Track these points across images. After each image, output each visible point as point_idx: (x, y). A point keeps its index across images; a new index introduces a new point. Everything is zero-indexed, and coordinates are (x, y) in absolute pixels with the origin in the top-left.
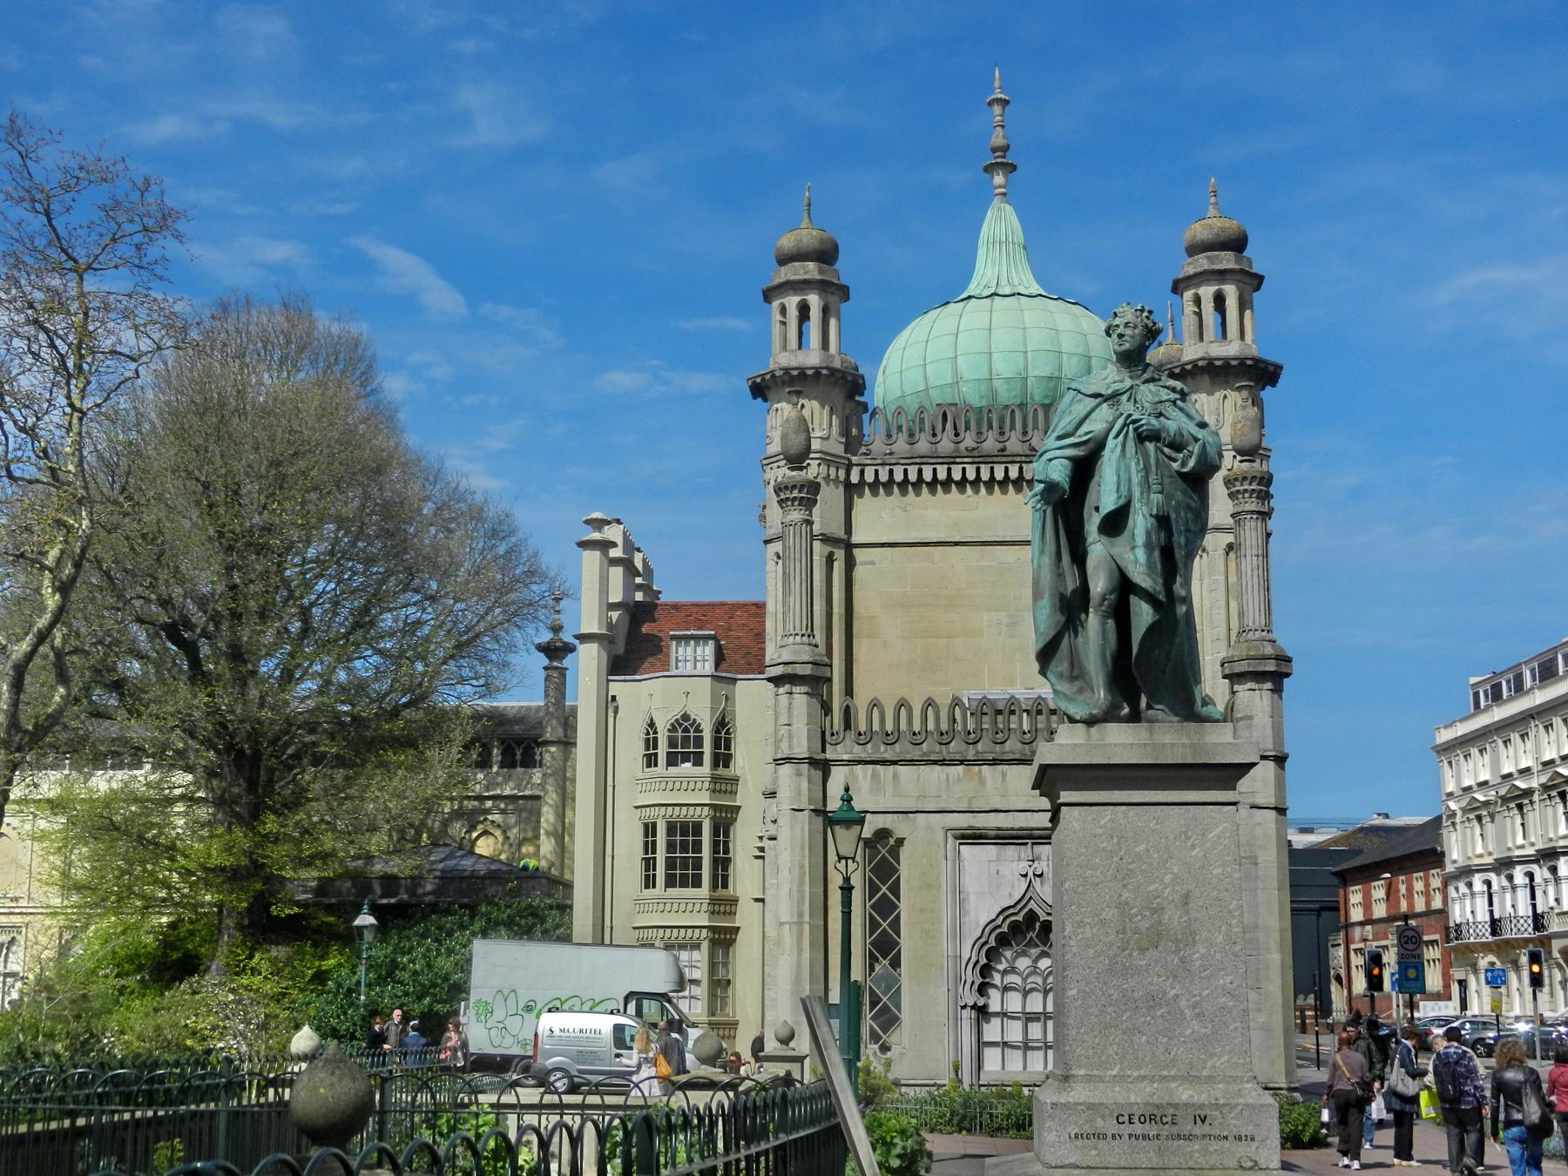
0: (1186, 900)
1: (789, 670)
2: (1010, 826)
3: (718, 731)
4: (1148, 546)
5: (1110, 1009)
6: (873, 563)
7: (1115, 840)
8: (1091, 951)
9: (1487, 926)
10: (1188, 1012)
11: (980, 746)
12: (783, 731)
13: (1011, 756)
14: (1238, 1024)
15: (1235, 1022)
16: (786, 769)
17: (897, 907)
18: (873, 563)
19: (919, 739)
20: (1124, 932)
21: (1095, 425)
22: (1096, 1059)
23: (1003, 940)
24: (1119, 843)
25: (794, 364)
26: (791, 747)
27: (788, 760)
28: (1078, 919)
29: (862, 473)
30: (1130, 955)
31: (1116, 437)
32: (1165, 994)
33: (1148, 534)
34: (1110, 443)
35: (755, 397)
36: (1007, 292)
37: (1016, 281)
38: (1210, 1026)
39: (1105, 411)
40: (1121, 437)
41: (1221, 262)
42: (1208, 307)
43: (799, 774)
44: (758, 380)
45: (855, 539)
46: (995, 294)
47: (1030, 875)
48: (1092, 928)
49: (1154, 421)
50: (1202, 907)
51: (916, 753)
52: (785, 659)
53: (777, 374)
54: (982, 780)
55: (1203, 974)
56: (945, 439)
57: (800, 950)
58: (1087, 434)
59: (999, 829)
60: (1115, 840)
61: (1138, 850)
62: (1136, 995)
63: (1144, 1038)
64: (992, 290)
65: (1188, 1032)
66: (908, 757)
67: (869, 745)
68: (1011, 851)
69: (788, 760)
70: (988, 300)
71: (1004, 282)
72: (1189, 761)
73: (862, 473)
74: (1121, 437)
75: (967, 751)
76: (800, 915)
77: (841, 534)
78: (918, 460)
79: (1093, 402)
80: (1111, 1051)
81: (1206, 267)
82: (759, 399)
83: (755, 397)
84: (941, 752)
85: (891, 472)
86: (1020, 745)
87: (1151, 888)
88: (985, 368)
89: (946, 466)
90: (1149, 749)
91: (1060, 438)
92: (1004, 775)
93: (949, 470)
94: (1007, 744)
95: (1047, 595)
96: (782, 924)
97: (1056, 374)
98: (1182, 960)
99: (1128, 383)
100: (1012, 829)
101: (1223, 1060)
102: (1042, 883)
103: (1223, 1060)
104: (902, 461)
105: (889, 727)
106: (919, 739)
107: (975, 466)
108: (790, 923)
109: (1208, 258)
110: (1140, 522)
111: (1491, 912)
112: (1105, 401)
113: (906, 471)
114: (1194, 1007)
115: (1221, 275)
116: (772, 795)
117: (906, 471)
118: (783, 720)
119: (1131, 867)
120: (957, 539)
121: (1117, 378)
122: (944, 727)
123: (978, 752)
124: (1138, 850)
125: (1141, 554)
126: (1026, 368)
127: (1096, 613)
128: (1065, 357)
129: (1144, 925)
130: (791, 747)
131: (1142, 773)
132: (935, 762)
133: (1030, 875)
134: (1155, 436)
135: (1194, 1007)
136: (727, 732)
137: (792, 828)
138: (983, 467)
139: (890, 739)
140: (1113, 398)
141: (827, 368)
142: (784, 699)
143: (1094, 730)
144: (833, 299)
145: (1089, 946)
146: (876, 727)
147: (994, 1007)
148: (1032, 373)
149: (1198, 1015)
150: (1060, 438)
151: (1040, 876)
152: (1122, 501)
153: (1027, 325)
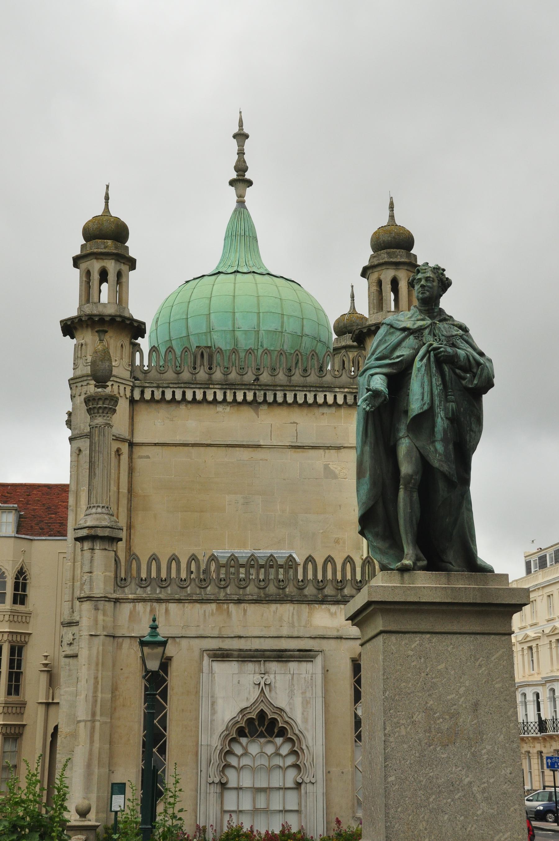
0: (476, 706)
1: (93, 532)
2: (249, 648)
3: (17, 578)
4: (445, 440)
5: (420, 793)
6: (148, 457)
7: (422, 660)
8: (405, 746)
9: (536, 725)
10: (479, 796)
11: (228, 590)
12: (86, 577)
13: (250, 597)
14: (517, 806)
15: (515, 804)
16: (87, 606)
17: (165, 708)
18: (148, 457)
19: (185, 584)
20: (430, 732)
21: (404, 352)
22: (411, 833)
23: (241, 732)
24: (425, 662)
25: (95, 312)
26: (91, 589)
27: (89, 598)
28: (395, 720)
29: (142, 393)
30: (435, 749)
31: (421, 360)
32: (461, 781)
33: (445, 431)
34: (417, 364)
35: (65, 335)
36: (245, 271)
37: (251, 263)
38: (495, 807)
39: (411, 341)
40: (425, 360)
41: (396, 257)
42: (387, 287)
43: (97, 609)
44: (69, 323)
45: (136, 440)
46: (238, 272)
47: (262, 684)
48: (406, 728)
49: (449, 349)
50: (487, 713)
51: (181, 595)
52: (89, 524)
53: (83, 319)
54: (229, 614)
55: (490, 766)
56: (202, 371)
57: (92, 742)
58: (398, 357)
59: (241, 650)
60: (422, 660)
61: (439, 667)
62: (440, 781)
63: (446, 817)
64: (235, 269)
65: (479, 812)
66: (177, 597)
67: (149, 588)
68: (250, 667)
69: (89, 598)
70: (232, 276)
71: (242, 263)
72: (478, 601)
73: (142, 393)
74: (425, 360)
75: (219, 593)
76: (94, 714)
77: (127, 435)
78: (182, 385)
79: (399, 336)
80: (421, 827)
81: (386, 260)
82: (68, 337)
83: (65, 335)
84: (200, 594)
85: (163, 393)
86: (256, 590)
87: (449, 697)
88: (230, 323)
89: (202, 391)
90: (449, 592)
91: (377, 359)
92: (245, 611)
93: (205, 393)
94: (248, 589)
95: (368, 475)
96: (79, 722)
97: (280, 330)
98: (473, 755)
99: (428, 322)
100: (250, 650)
101: (506, 836)
102: (270, 691)
103: (506, 836)
104: (171, 385)
105: (144, 575)
106: (185, 584)
107: (223, 391)
108: (85, 721)
109: (388, 253)
110: (441, 423)
111: (539, 715)
112: (411, 334)
113: (174, 393)
114: (483, 793)
115: (397, 265)
116: (70, 624)
117: (174, 393)
118: (86, 569)
119: (434, 680)
120: (209, 442)
121: (419, 317)
122: (183, 575)
123: (227, 594)
124: (439, 667)
125: (439, 446)
126: (259, 325)
127: (405, 489)
128: (285, 317)
129: (445, 726)
130: (91, 589)
131: (444, 608)
132: (196, 601)
133: (262, 684)
134: (452, 360)
135: (483, 793)
136: (25, 579)
137: (90, 648)
138: (228, 392)
139: (163, 583)
140: (417, 332)
141: (120, 316)
142: (87, 554)
143: (406, 576)
144: (124, 268)
145: (404, 742)
146: (154, 575)
147: (232, 783)
148: (263, 328)
149: (486, 799)
150: (377, 359)
151: (269, 684)
152: (426, 407)
153: (260, 294)
